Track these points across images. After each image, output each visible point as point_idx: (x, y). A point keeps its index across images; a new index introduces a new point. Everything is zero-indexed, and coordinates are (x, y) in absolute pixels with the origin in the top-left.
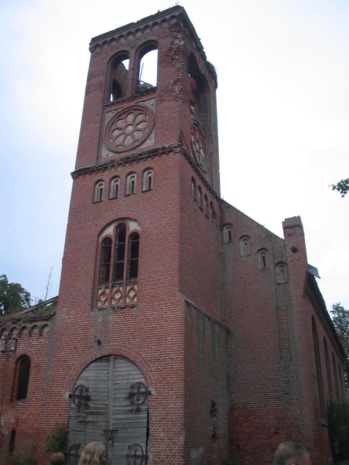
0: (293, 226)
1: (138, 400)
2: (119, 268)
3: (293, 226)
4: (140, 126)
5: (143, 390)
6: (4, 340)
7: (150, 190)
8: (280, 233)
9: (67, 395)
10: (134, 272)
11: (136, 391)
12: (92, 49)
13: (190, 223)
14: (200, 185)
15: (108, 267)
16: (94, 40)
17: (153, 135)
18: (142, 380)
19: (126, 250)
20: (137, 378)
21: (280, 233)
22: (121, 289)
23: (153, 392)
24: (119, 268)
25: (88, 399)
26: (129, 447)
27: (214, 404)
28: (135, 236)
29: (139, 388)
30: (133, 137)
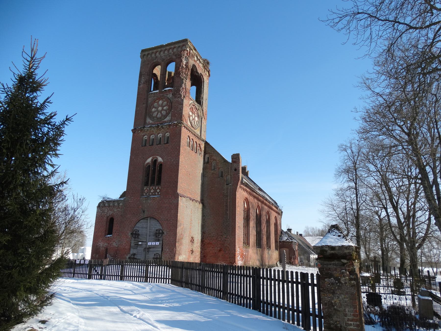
0: (236, 158)
1: (159, 236)
2: (153, 179)
3: (236, 158)
4: (165, 108)
5: (161, 232)
6: (433, 275)
7: (167, 143)
8: (230, 160)
9: (130, 234)
10: (159, 183)
11: (158, 232)
12: (142, 56)
13: (185, 159)
14: (193, 138)
15: (148, 178)
16: (143, 51)
17: (170, 115)
18: (161, 228)
19: (156, 171)
20: (159, 227)
21: (230, 160)
22: (154, 188)
23: (165, 233)
24: (153, 179)
25: (139, 235)
26: (155, 255)
27: (192, 238)
28: (161, 165)
29: (159, 231)
30: (161, 113)
